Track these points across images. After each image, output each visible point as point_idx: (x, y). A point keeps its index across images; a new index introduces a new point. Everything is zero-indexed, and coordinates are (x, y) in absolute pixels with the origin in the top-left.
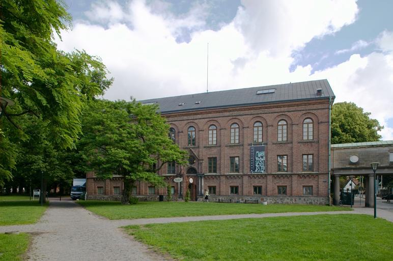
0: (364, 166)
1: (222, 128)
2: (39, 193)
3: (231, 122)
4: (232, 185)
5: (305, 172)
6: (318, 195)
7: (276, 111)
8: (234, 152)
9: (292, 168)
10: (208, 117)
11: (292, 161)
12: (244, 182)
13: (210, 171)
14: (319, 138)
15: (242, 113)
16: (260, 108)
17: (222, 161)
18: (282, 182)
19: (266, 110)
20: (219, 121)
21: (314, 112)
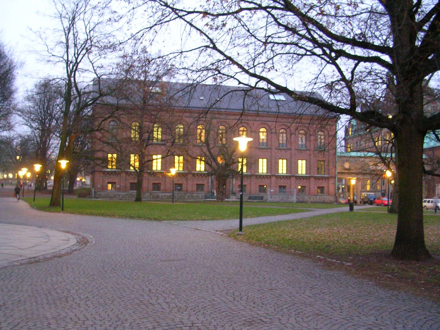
13: (318, 173)
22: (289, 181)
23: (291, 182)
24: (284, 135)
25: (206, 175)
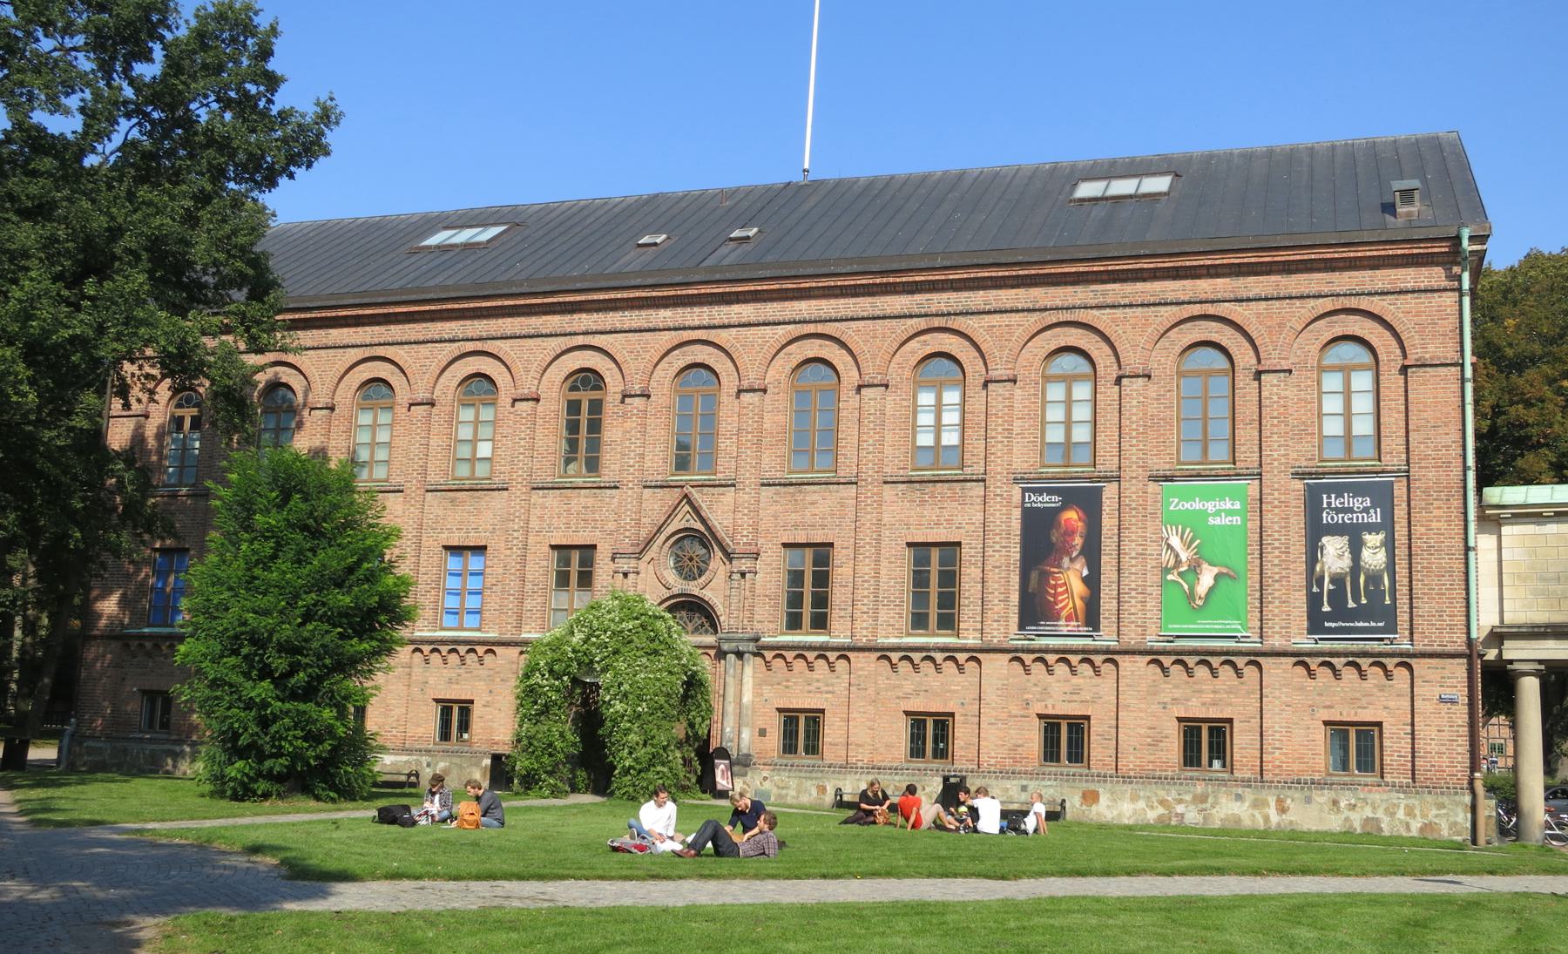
1: (867, 379)
2: (170, 761)
3: (919, 348)
4: (918, 705)
5: (155, 630)
6: (1415, 781)
7: (1170, 297)
8: (930, 513)
10: (788, 316)
12: (990, 695)
17: (866, 569)
18: (1206, 696)
19: (1116, 286)
22: (1106, 684)
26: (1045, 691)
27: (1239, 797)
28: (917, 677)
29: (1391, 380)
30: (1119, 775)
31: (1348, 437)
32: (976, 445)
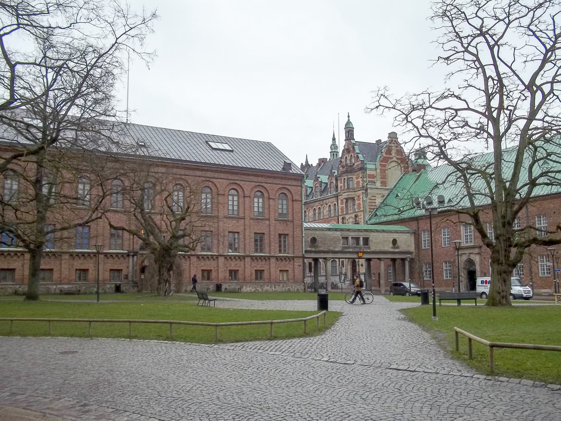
0: (321, 249)
9: (270, 250)
11: (270, 241)
13: (256, 251)
14: (293, 217)
15: (216, 175)
16: (269, 177)
18: (259, 266)
20: (189, 181)
21: (289, 187)
22: (242, 263)
23: (245, 264)
24: (236, 198)
25: (125, 256)
26: (231, 265)
27: (268, 286)
28: (204, 262)
29: (290, 203)
30: (270, 282)
31: (233, 210)
32: (266, 211)
